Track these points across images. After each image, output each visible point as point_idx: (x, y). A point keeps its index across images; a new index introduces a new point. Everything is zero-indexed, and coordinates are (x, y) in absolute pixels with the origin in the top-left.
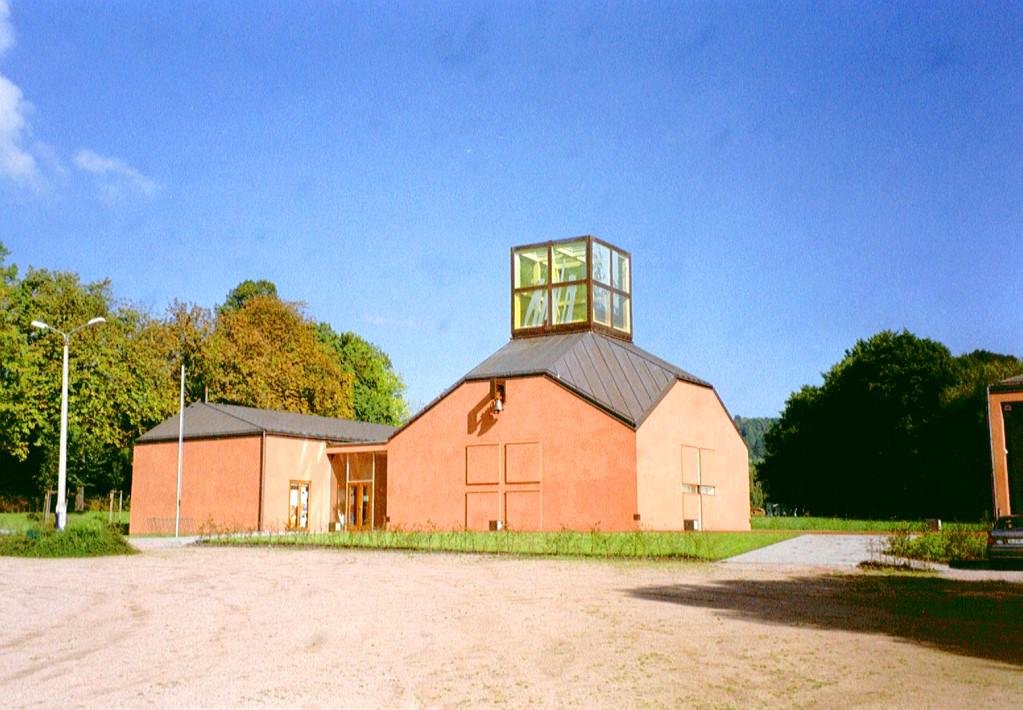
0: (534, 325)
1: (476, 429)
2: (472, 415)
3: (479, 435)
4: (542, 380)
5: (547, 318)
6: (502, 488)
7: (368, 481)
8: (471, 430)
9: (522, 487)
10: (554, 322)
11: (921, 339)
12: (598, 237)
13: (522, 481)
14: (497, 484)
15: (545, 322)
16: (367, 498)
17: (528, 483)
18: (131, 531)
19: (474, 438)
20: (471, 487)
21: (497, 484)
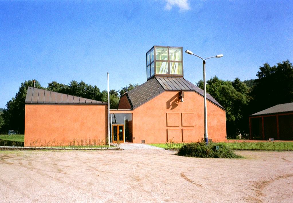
0: (163, 73)
1: (170, 107)
2: (168, 103)
3: (171, 110)
4: (194, 93)
5: (168, 71)
6: (181, 127)
7: (263, 119)
8: (168, 108)
9: (188, 128)
10: (171, 74)
11: (254, 77)
12: (157, 45)
13: (188, 125)
14: (179, 126)
15: (167, 73)
16: (121, 131)
17: (190, 126)
18: (136, 134)
19: (169, 111)
20: (168, 127)
21: (179, 126)
